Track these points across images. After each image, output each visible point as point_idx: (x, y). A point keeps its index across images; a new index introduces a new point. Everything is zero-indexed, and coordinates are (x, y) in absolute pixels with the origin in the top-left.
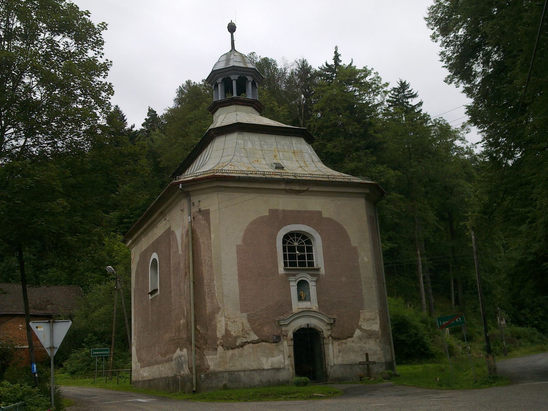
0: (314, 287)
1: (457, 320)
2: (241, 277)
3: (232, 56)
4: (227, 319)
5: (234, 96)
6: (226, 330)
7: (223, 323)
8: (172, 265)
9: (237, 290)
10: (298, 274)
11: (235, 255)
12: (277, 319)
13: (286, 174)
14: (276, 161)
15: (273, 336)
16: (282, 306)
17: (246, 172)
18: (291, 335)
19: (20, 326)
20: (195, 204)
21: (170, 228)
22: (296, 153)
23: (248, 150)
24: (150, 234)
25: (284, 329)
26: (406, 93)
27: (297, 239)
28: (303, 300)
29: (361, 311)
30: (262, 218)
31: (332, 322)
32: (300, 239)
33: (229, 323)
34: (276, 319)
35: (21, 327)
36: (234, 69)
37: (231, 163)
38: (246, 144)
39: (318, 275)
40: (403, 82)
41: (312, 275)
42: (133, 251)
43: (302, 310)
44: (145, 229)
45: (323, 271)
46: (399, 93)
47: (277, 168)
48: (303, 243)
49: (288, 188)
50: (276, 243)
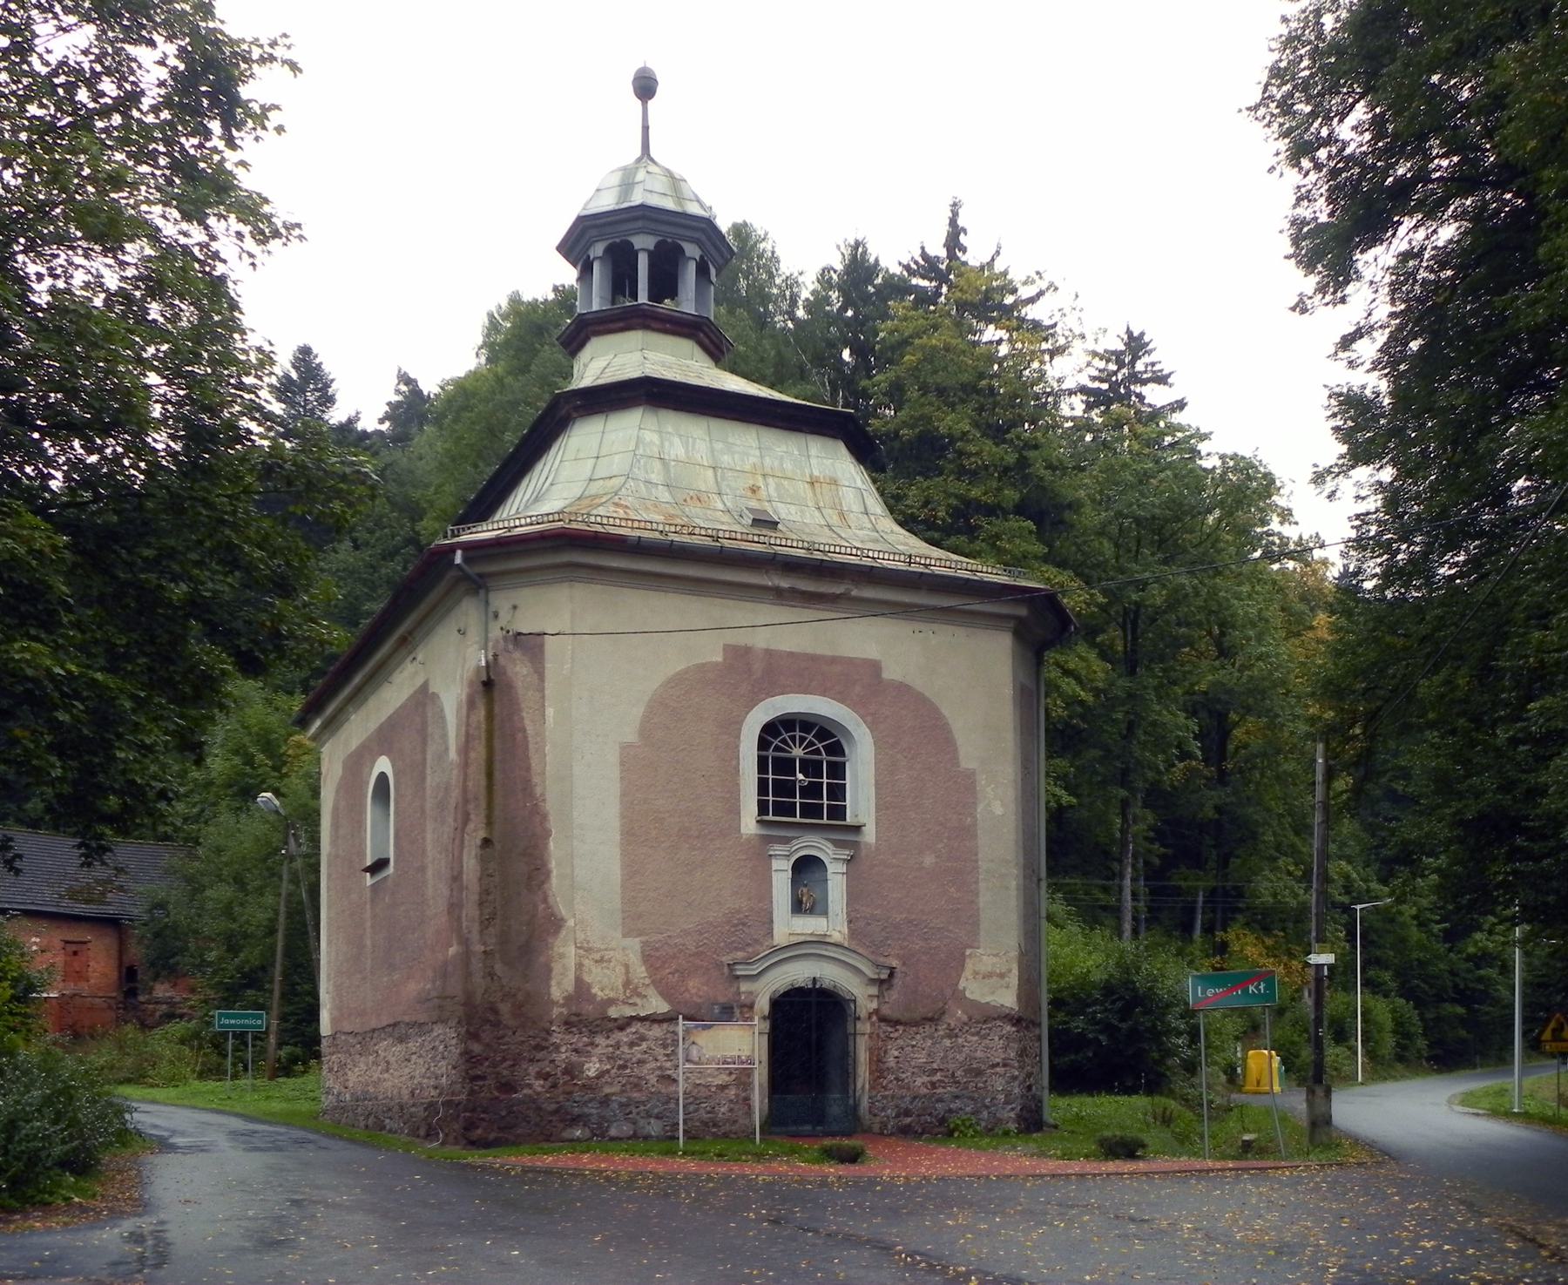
2: (631, 835)
3: (641, 175)
4: (581, 951)
5: (640, 301)
6: (579, 981)
7: (571, 962)
8: (428, 792)
10: (794, 838)
11: (615, 773)
12: (727, 959)
14: (754, 504)
15: (713, 1004)
16: (744, 924)
17: (661, 528)
18: (763, 1005)
20: (501, 614)
21: (425, 686)
24: (372, 703)
25: (744, 987)
26: (1139, 366)
27: (802, 739)
29: (968, 952)
30: (701, 668)
31: (884, 976)
32: (810, 737)
33: (586, 962)
34: (724, 959)
36: (646, 215)
37: (616, 499)
38: (667, 444)
39: (855, 845)
40: (1136, 334)
41: (838, 844)
42: (326, 750)
43: (802, 939)
44: (359, 689)
45: (869, 835)
46: (1121, 365)
48: (817, 752)
49: (785, 584)
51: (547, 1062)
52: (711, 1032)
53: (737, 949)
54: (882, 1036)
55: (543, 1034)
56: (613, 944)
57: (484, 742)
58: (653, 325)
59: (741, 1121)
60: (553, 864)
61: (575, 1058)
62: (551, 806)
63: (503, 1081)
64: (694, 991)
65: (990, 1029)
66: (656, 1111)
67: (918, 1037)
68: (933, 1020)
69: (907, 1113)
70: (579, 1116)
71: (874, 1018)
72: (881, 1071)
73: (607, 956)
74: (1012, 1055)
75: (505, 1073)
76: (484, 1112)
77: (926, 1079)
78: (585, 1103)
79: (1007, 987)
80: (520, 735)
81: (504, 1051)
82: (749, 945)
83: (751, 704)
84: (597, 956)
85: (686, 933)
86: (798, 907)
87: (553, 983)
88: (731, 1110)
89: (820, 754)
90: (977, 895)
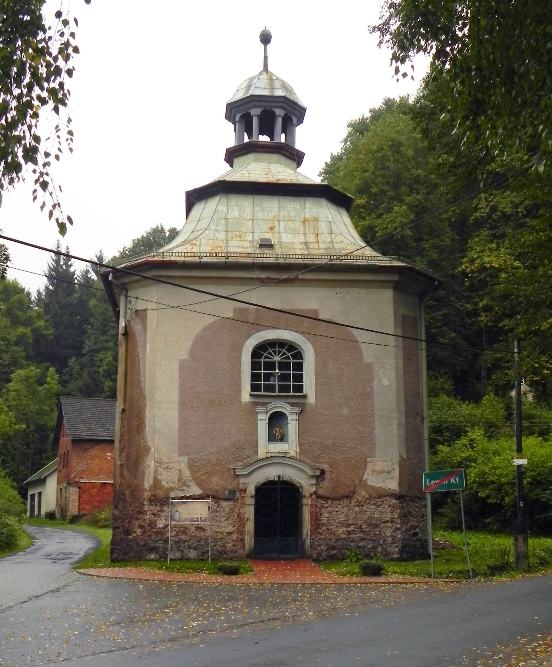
0: (294, 422)
1: (452, 480)
2: (183, 405)
4: (157, 464)
6: (155, 479)
7: (152, 469)
9: (175, 424)
10: (270, 403)
11: (177, 374)
12: (232, 466)
13: (262, 256)
16: (242, 448)
18: (251, 490)
19: (108, 454)
22: (306, 222)
23: (231, 220)
25: (242, 480)
28: (277, 441)
29: (369, 460)
32: (284, 351)
33: (159, 469)
35: (110, 456)
38: (230, 211)
39: (303, 405)
41: (292, 405)
43: (273, 455)
45: (312, 399)
47: (261, 246)
48: (288, 358)
50: (240, 358)
51: (142, 520)
52: (186, 505)
53: (238, 461)
54: (319, 505)
55: (141, 506)
56: (174, 460)
57: (124, 362)
58: (258, 150)
59: (239, 551)
60: (147, 421)
61: (153, 518)
62: (147, 393)
63: (126, 529)
64: (215, 483)
65: (383, 502)
66: (194, 545)
67: (340, 506)
68: (349, 497)
69: (333, 548)
70: (153, 548)
71: (314, 496)
72: (319, 525)
73: (171, 465)
74: (396, 516)
75: (127, 525)
76: (118, 545)
77: (345, 529)
78: (157, 541)
79: (392, 479)
80: (137, 358)
81: (127, 514)
82: (245, 459)
83: (248, 336)
84: (165, 466)
85: (212, 453)
86: (272, 438)
87: (145, 480)
88: (234, 545)
89: (289, 359)
90: (374, 428)
